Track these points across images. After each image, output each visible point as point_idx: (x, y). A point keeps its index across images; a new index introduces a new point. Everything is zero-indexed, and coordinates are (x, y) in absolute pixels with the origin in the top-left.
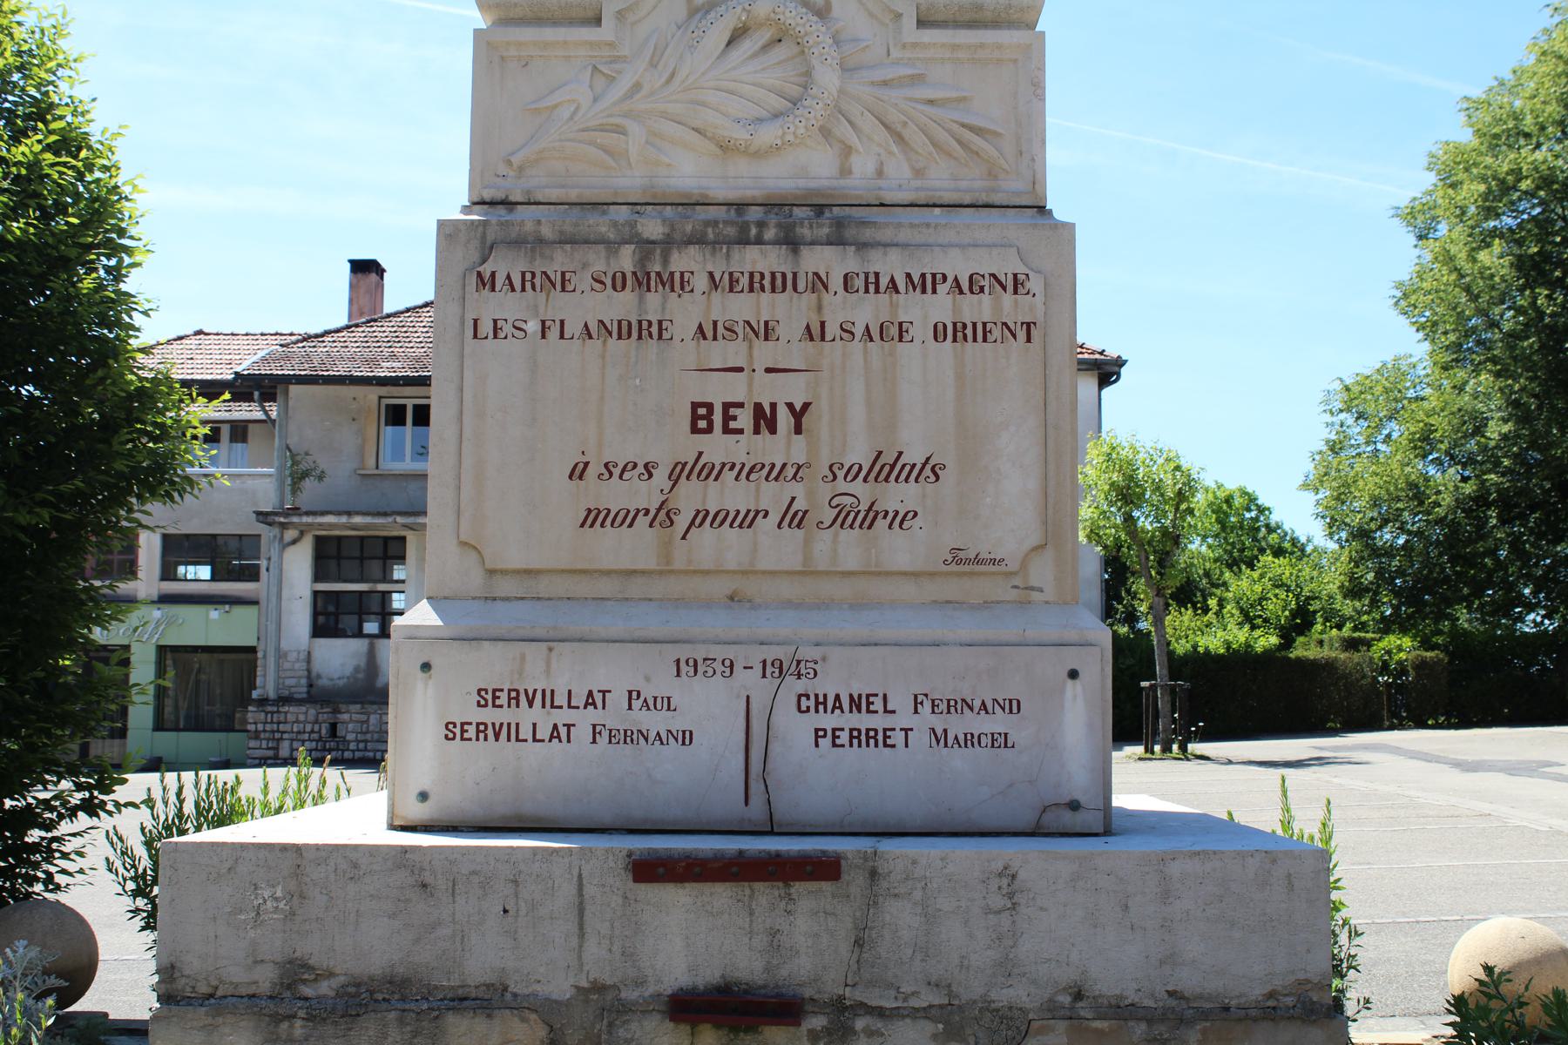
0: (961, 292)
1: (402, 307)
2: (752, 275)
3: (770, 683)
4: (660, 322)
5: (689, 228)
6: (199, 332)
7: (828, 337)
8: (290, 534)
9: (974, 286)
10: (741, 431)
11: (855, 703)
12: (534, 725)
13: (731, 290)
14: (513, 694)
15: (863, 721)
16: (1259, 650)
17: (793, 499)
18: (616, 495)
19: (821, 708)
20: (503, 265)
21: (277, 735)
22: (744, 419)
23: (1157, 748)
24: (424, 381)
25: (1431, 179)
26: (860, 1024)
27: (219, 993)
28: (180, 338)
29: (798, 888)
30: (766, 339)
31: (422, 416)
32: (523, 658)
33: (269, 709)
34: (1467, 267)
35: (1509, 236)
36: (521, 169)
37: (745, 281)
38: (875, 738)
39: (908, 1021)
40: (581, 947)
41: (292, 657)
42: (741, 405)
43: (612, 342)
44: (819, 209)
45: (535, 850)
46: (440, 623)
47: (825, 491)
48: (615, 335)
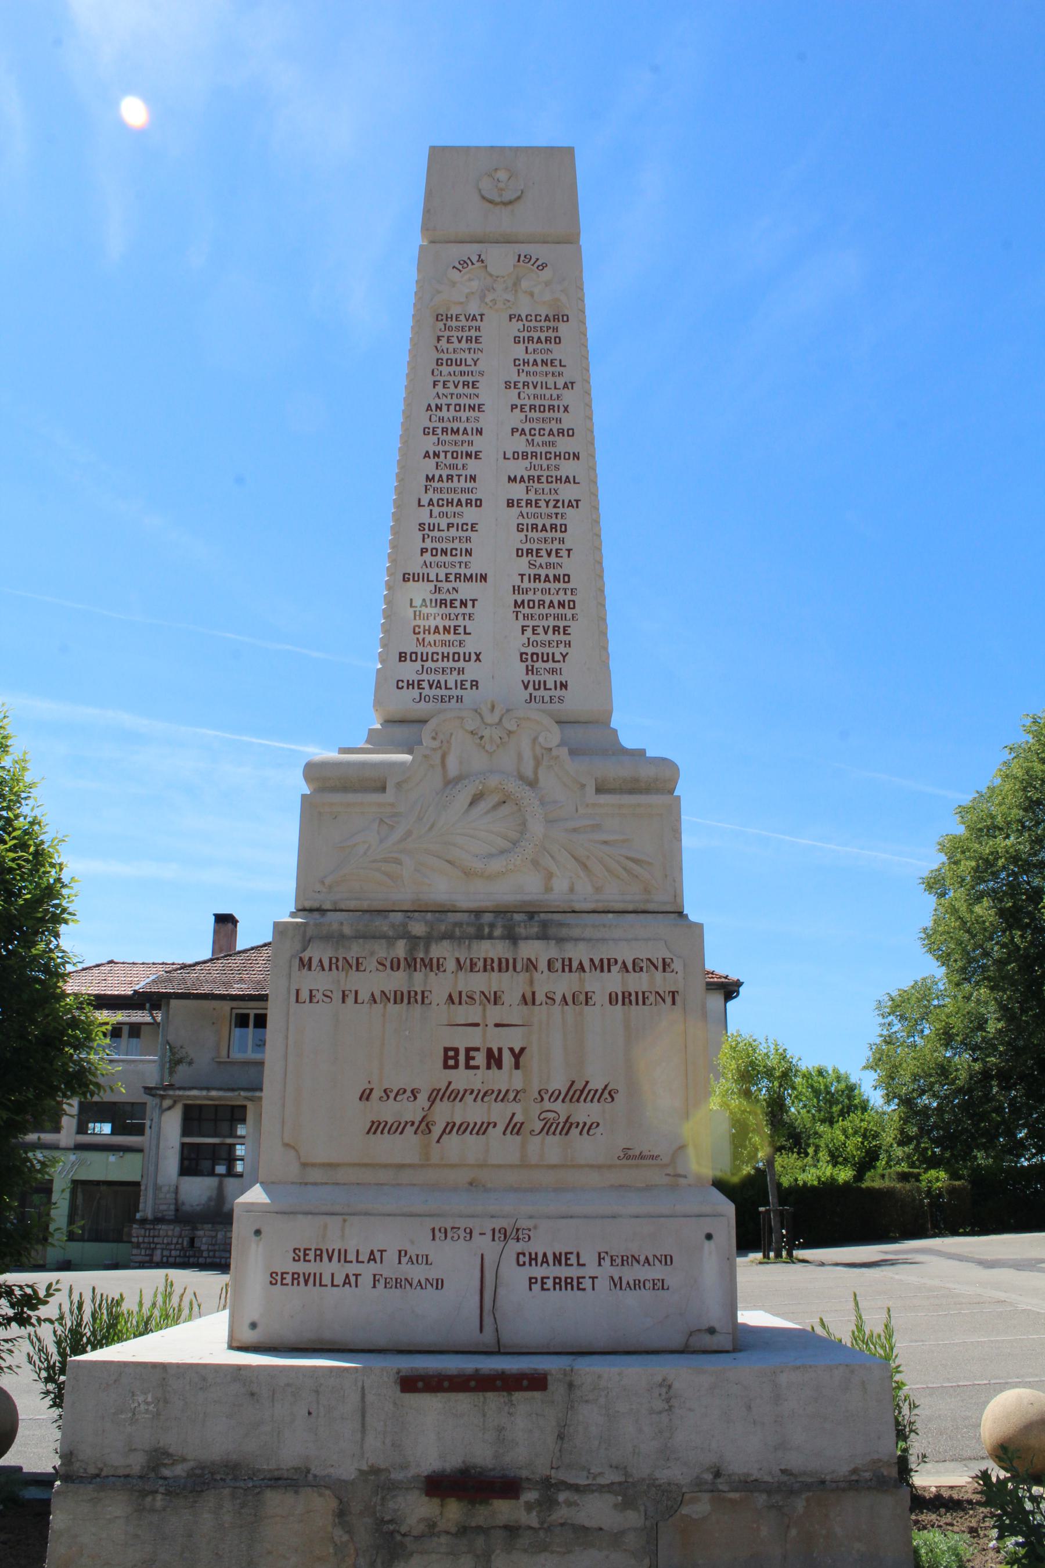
0: (627, 971)
1: (248, 947)
2: (485, 960)
3: (498, 1245)
4: (423, 992)
5: (443, 928)
6: (111, 962)
7: (537, 1002)
8: (167, 1103)
9: (636, 966)
10: (477, 1067)
11: (557, 1259)
12: (333, 1275)
13: (471, 971)
14: (318, 1252)
15: (563, 1272)
16: (841, 1181)
17: (514, 1114)
18: (389, 1111)
19: (533, 1262)
20: (317, 952)
21: (152, 1246)
22: (480, 1059)
23: (772, 1254)
24: (264, 998)
25: (944, 858)
26: (562, 1497)
27: (104, 1474)
28: (98, 966)
29: (517, 1396)
30: (495, 1004)
31: (261, 1021)
32: (325, 1227)
33: (148, 1226)
34: (967, 916)
35: (993, 894)
36: (330, 887)
37: (481, 964)
38: (571, 1283)
39: (596, 1494)
40: (363, 1440)
41: (165, 1189)
42: (477, 1049)
43: (391, 1006)
44: (531, 915)
45: (331, 1369)
46: (268, 1201)
47: (536, 1109)
48: (392, 1001)
